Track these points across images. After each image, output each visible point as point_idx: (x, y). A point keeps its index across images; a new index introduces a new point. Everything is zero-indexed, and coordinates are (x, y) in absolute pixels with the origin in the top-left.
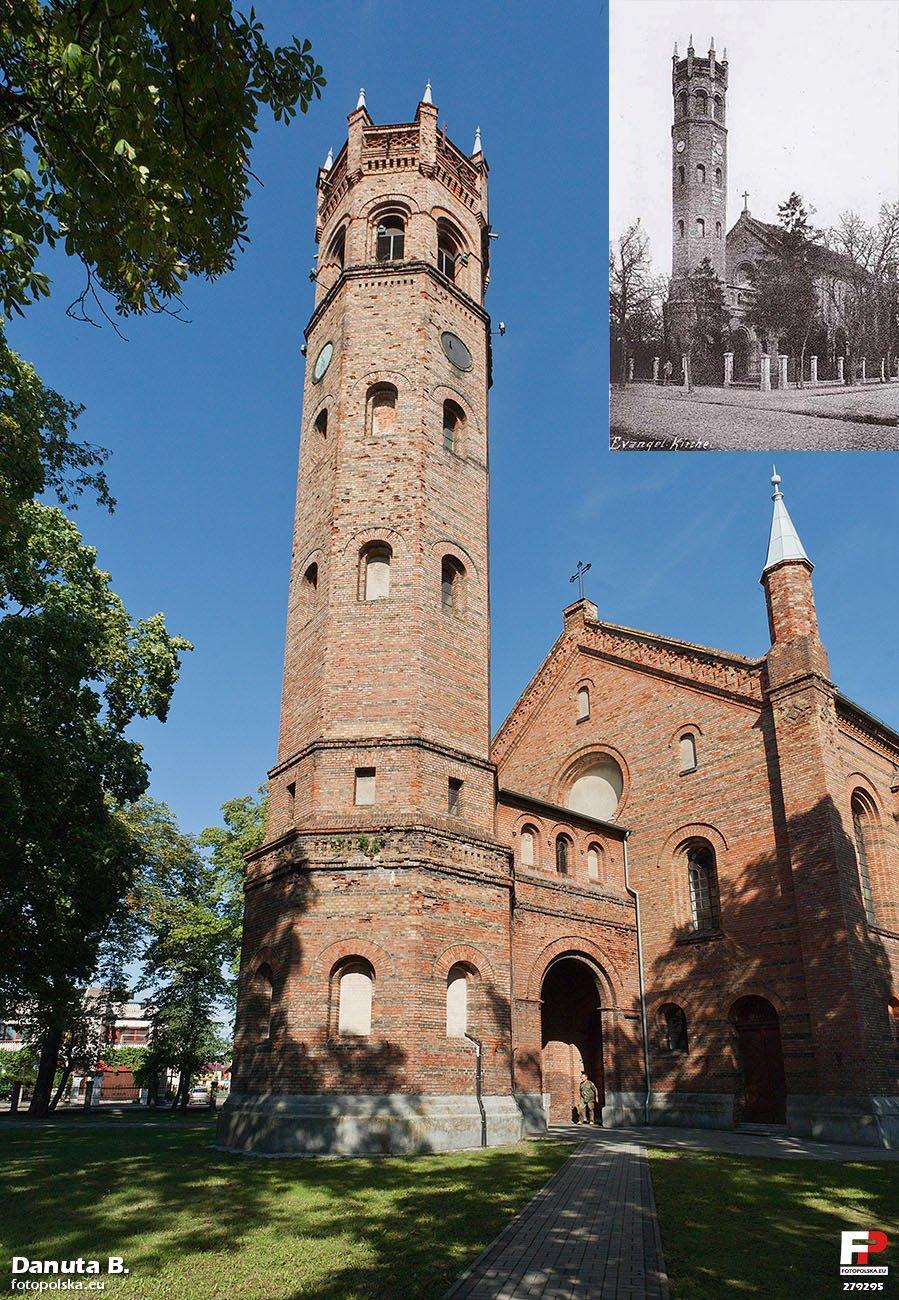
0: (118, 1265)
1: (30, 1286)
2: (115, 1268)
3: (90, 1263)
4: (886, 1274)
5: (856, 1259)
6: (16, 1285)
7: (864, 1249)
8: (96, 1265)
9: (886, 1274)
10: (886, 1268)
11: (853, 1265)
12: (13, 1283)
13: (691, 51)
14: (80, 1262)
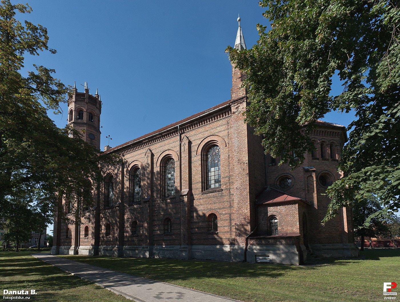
0: (34, 292)
1: (8, 298)
2: (33, 293)
3: (26, 291)
4: (396, 294)
5: (389, 290)
6: (4, 298)
7: (390, 287)
8: (27, 292)
9: (396, 294)
10: (396, 293)
11: (387, 292)
12: (4, 297)
13: (87, 90)
14: (23, 291)
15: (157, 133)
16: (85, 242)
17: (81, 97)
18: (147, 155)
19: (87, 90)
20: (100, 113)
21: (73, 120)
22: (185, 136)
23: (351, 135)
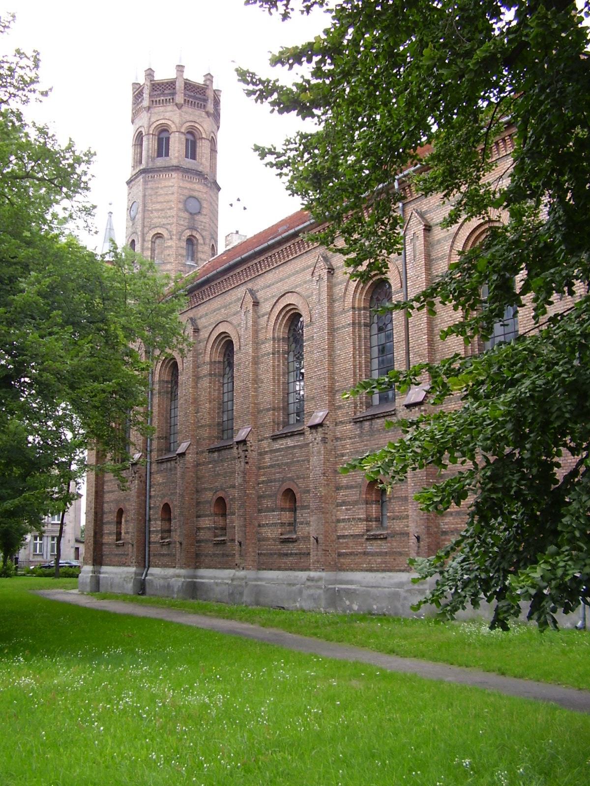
15: (306, 224)
16: (163, 555)
17: (166, 92)
18: (317, 274)
19: (180, 68)
20: (218, 127)
21: (143, 162)
22: (414, 212)
23: (495, 288)
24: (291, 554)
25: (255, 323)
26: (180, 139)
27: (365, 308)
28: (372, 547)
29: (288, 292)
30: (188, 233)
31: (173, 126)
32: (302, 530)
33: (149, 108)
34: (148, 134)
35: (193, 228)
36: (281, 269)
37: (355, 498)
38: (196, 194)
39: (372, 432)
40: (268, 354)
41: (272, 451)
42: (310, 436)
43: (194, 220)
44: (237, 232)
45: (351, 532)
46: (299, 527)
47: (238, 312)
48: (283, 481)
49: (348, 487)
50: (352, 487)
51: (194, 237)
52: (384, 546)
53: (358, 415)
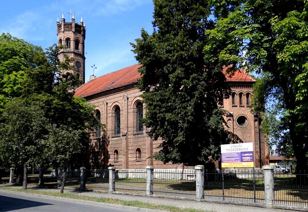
24: (117, 165)
25: (107, 108)
26: (74, 43)
27: (205, 195)
28: (137, 163)
29: (116, 102)
30: (77, 73)
31: (71, 38)
32: (119, 160)
33: (64, 32)
34: (64, 40)
35: (78, 71)
36: (114, 95)
37: (133, 152)
38: (79, 61)
39: (138, 138)
40: (110, 116)
41: (111, 141)
42: (122, 137)
43: (79, 69)
44: (93, 75)
45: (132, 160)
46: (119, 159)
47: (101, 105)
48: (115, 148)
49: (131, 150)
50: (133, 150)
51: (79, 74)
52: (140, 163)
53: (134, 133)
